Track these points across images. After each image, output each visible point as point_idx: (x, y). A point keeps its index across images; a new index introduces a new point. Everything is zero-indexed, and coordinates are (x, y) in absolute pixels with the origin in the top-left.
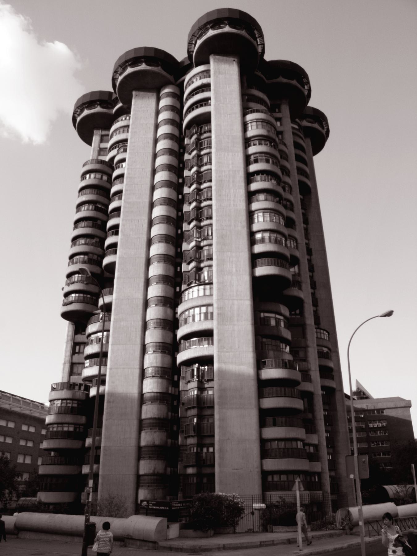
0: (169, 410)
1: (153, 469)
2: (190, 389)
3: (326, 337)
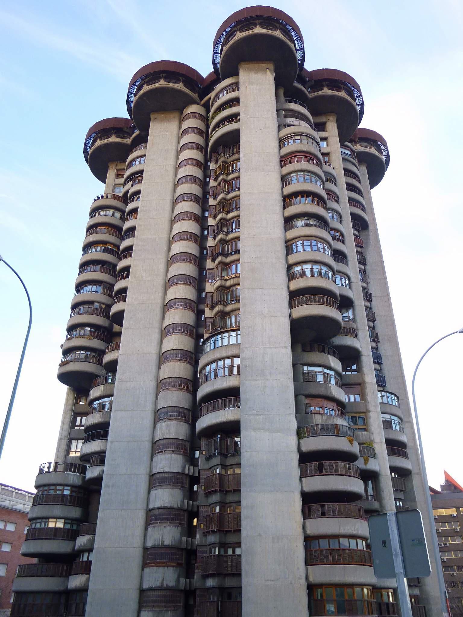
0: (182, 535)
1: (161, 579)
3: (395, 403)
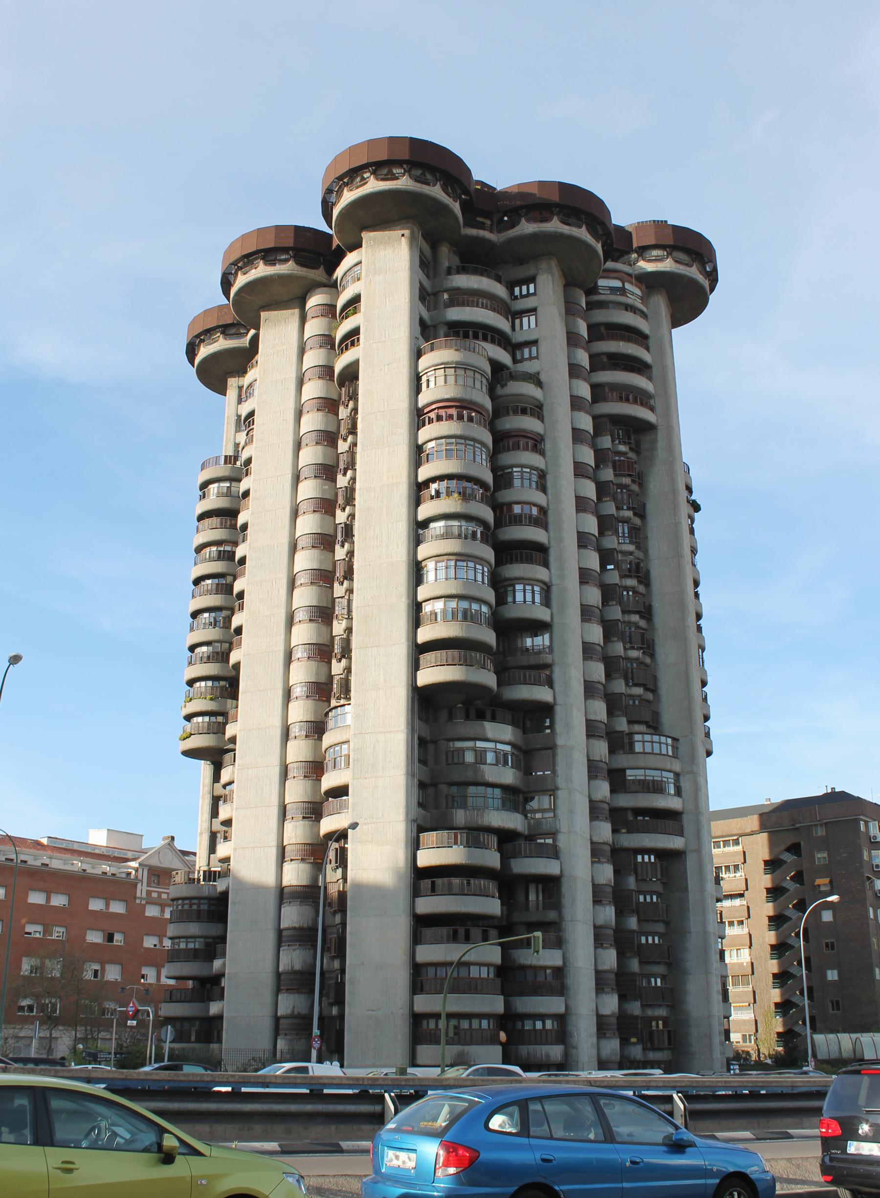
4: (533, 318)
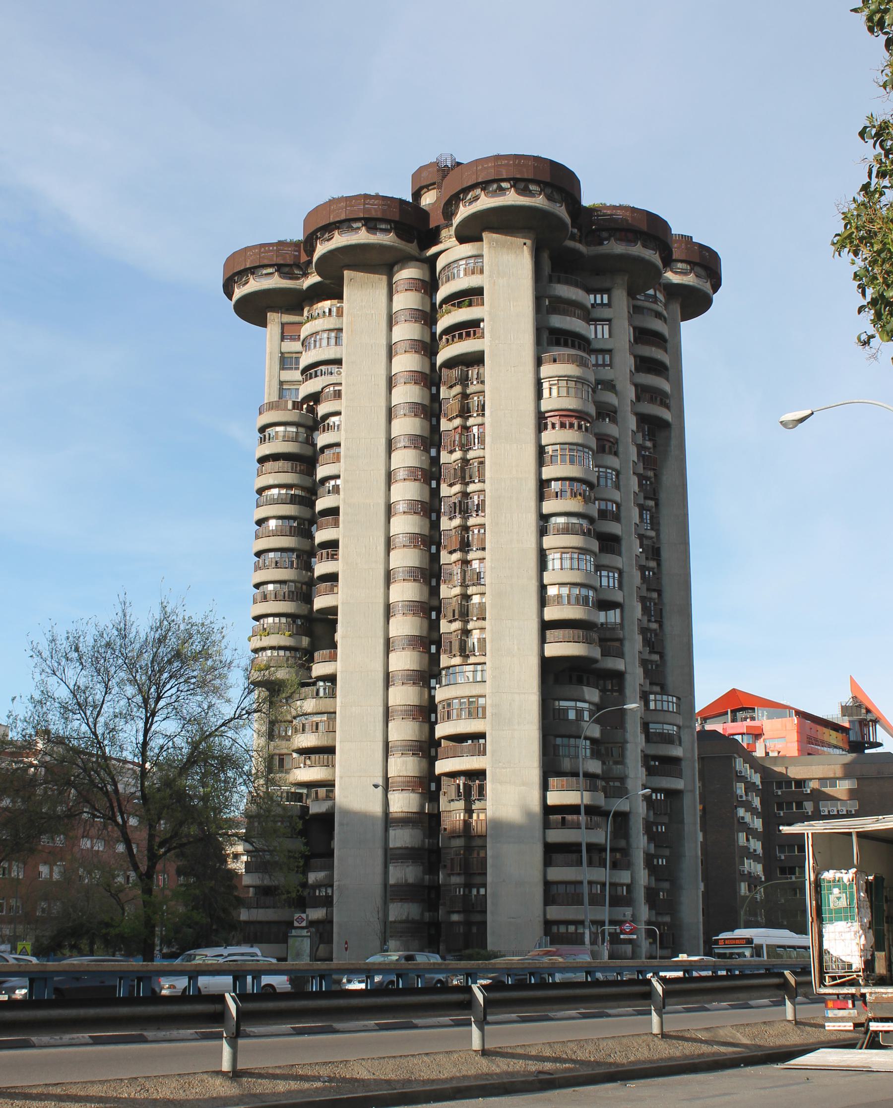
0: (424, 873)
2: (453, 812)
4: (606, 328)
